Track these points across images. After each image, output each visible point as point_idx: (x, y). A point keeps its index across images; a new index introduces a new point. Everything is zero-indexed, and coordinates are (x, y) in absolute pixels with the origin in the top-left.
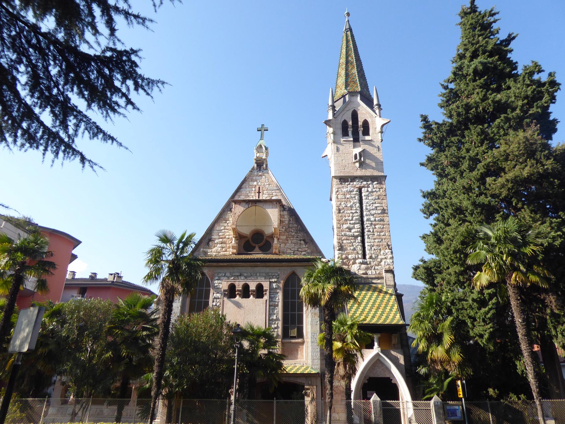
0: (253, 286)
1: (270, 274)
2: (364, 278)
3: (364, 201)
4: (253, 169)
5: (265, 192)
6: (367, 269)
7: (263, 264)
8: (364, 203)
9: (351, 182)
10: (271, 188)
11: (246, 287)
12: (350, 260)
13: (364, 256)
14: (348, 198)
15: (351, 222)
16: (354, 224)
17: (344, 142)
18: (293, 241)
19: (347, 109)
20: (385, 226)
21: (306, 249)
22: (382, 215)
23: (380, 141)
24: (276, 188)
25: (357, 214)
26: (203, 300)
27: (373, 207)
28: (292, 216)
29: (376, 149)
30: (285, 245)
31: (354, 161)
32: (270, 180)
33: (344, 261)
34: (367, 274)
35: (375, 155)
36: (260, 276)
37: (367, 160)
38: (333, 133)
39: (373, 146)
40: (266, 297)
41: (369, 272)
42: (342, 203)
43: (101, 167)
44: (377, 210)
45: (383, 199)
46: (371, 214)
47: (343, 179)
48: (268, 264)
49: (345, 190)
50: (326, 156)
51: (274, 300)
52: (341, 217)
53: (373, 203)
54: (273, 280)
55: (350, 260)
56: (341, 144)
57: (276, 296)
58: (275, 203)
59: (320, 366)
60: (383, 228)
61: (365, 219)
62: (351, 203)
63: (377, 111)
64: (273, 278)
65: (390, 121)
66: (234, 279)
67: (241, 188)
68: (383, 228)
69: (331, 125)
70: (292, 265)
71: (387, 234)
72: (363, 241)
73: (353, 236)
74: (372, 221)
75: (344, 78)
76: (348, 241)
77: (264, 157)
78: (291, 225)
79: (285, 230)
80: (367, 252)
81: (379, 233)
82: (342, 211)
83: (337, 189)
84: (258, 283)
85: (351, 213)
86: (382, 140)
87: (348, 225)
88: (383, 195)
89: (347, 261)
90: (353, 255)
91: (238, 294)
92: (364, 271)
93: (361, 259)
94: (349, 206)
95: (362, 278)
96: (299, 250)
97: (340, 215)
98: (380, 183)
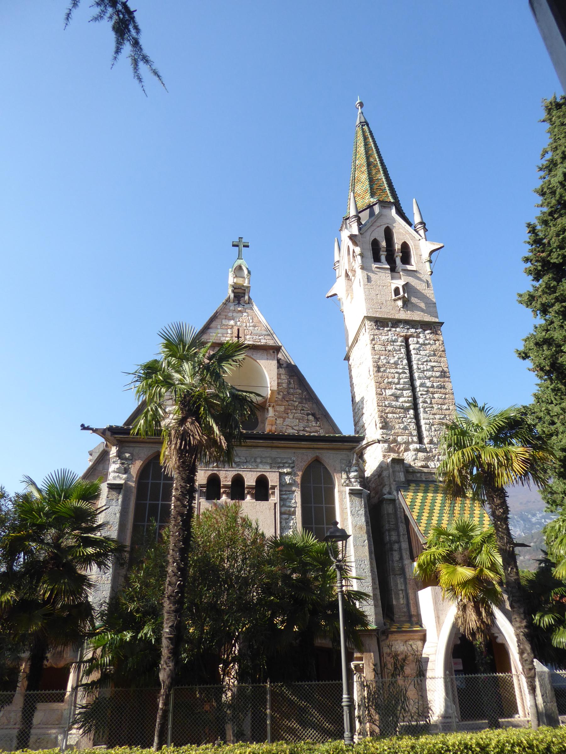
0: (250, 479)
1: (279, 460)
2: (425, 473)
3: (414, 357)
4: (228, 300)
5: (248, 337)
6: (427, 459)
7: (268, 443)
8: (413, 360)
9: (392, 327)
10: (258, 332)
11: (238, 481)
12: (400, 444)
13: (420, 440)
14: (389, 351)
15: (398, 386)
16: (402, 389)
17: (376, 269)
18: (296, 415)
19: (378, 224)
20: (447, 396)
21: (318, 428)
22: (442, 380)
23: (430, 273)
24: (265, 333)
25: (405, 375)
26: (160, 502)
27: (429, 367)
28: (293, 376)
29: (424, 284)
30: (284, 421)
31: (394, 297)
32: (255, 319)
33: (392, 445)
34: (428, 467)
35: (423, 292)
36: (261, 462)
37: (412, 298)
38: (360, 255)
39: (419, 279)
40: (275, 499)
41: (431, 464)
42: (382, 358)
43: (156, 73)
44: (433, 371)
45: (441, 357)
46: (426, 377)
47: (381, 322)
48: (276, 443)
49: (384, 338)
50: (335, 295)
51: (288, 504)
52: (381, 377)
53: (427, 361)
54: (285, 471)
55: (400, 444)
56: (373, 272)
57: (291, 496)
58: (271, 352)
59: (374, 617)
60: (445, 398)
61: (418, 383)
62: (396, 359)
63: (422, 232)
64: (283, 467)
65: (443, 247)
66: (217, 467)
67: (209, 328)
68: (445, 398)
69: (358, 243)
70: (315, 446)
71: (451, 408)
72: (417, 416)
73: (402, 408)
74: (428, 387)
75: (367, 183)
76: (395, 415)
77: (246, 284)
78: (292, 391)
79: (283, 398)
80: (425, 433)
81: (439, 406)
82: (382, 370)
83: (372, 336)
84: (259, 474)
85: (397, 373)
86: (432, 272)
87: (393, 391)
88: (441, 350)
89: (397, 446)
90: (404, 437)
91: (224, 492)
92: (424, 463)
93: (416, 443)
94: (392, 361)
95: (421, 472)
96: (306, 429)
97: (380, 374)
98: (435, 333)
